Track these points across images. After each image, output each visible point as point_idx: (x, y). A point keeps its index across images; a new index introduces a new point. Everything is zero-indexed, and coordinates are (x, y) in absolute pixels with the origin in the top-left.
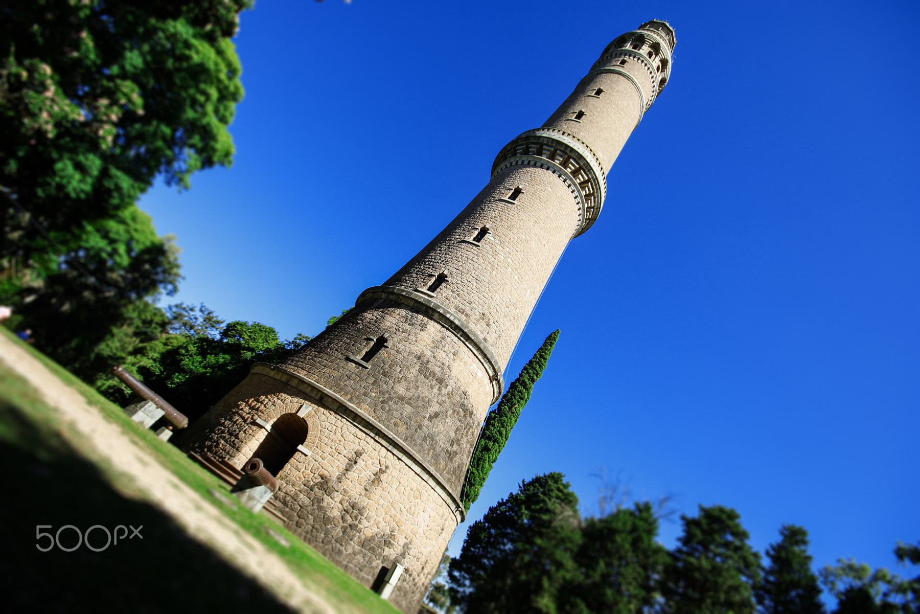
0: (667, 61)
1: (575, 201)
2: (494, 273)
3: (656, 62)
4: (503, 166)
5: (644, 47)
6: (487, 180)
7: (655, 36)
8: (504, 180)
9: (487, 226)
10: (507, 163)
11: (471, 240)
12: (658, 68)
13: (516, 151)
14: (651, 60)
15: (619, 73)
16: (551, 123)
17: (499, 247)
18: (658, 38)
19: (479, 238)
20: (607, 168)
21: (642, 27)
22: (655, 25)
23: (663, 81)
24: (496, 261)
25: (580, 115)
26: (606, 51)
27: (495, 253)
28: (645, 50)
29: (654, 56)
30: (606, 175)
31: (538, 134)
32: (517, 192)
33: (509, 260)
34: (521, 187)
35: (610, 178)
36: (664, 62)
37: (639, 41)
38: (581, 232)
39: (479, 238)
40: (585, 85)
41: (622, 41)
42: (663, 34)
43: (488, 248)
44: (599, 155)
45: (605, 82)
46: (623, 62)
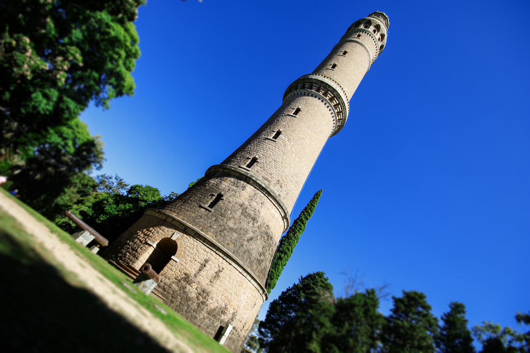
0: (384, 35)
2: (285, 157)
4: (289, 95)
5: (371, 27)
6: (280, 103)
7: (377, 21)
9: (281, 130)
10: (292, 94)
11: (271, 138)
12: (379, 39)
14: (375, 35)
16: (317, 71)
18: (379, 22)
19: (276, 137)
20: (350, 97)
21: (370, 15)
23: (382, 47)
25: (334, 66)
26: (349, 29)
27: (285, 145)
28: (371, 29)
29: (376, 32)
30: (349, 100)
31: (310, 77)
32: (298, 111)
33: (293, 149)
34: (300, 107)
35: (351, 102)
36: (383, 36)
37: (368, 24)
38: (334, 134)
39: (276, 137)
40: (337, 49)
41: (358, 23)
42: (382, 20)
43: (281, 143)
44: (345, 89)
45: (349, 47)
46: (359, 36)
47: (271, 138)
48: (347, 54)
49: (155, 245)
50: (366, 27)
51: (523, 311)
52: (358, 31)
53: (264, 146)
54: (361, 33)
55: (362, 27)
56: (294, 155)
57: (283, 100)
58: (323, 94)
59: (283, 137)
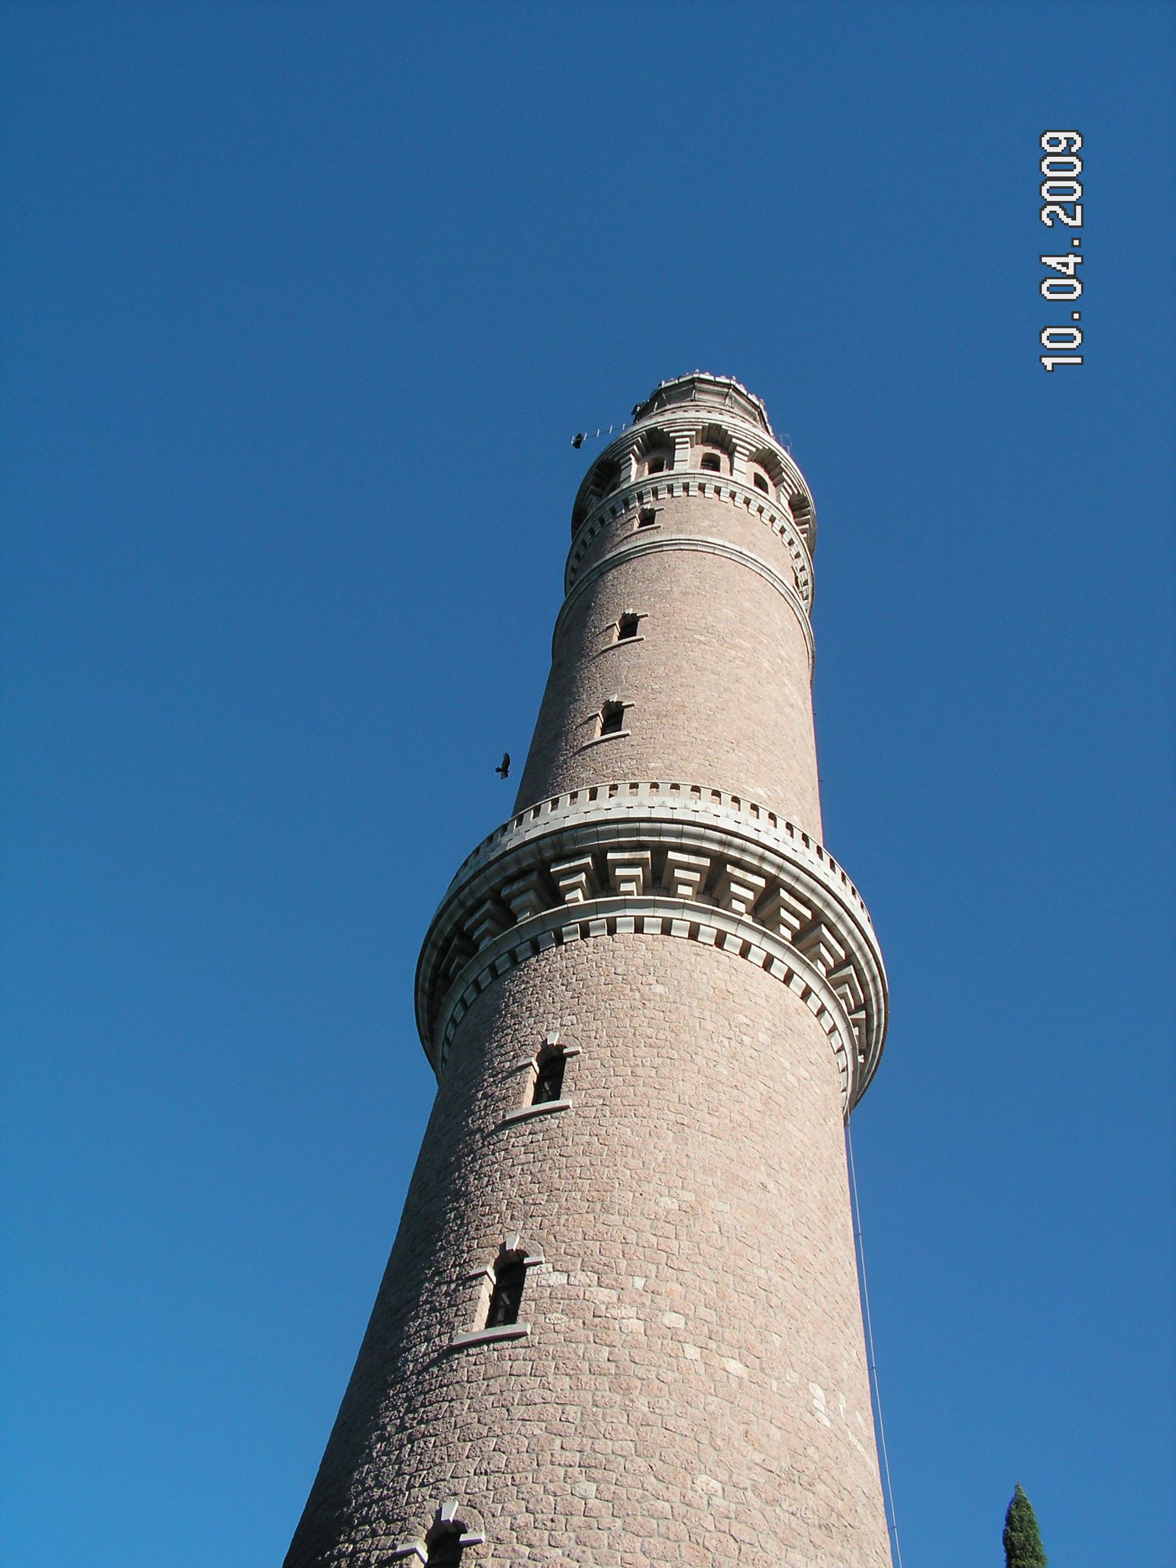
0: (772, 454)
1: (769, 984)
2: (642, 1404)
3: (745, 470)
4: (452, 1009)
5: (678, 455)
6: (422, 1087)
7: (691, 414)
8: (483, 1052)
9: (514, 1244)
10: (462, 991)
11: (527, 1105)
12: (759, 482)
13: (466, 936)
14: (724, 472)
15: (658, 546)
16: (541, 778)
17: (603, 1295)
18: (703, 414)
19: (506, 1305)
20: (810, 818)
21: (642, 413)
22: (685, 391)
23: (798, 506)
24: (622, 1354)
25: (614, 716)
26: (579, 516)
27: (598, 1323)
28: (688, 458)
29: (724, 459)
30: (817, 839)
31: (511, 841)
32: (553, 1064)
33: (670, 1319)
34: (554, 1039)
35: (838, 842)
36: (766, 459)
37: (659, 448)
38: (862, 1085)
39: (506, 1305)
40: (580, 620)
41: (607, 471)
42: (715, 401)
43: (563, 1322)
44: (756, 792)
45: (627, 591)
46: (648, 518)
47: (527, 1105)
48: (627, 716)
49: (423, 1550)
50: (656, 467)
51: (1051, 1539)
52: (626, 504)
53: (462, 1409)
54: (650, 503)
55: (636, 472)
56: (692, 1352)
57: (431, 1056)
58: (645, 890)
59: (558, 1279)
